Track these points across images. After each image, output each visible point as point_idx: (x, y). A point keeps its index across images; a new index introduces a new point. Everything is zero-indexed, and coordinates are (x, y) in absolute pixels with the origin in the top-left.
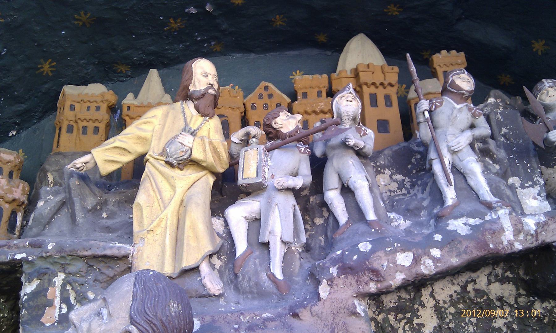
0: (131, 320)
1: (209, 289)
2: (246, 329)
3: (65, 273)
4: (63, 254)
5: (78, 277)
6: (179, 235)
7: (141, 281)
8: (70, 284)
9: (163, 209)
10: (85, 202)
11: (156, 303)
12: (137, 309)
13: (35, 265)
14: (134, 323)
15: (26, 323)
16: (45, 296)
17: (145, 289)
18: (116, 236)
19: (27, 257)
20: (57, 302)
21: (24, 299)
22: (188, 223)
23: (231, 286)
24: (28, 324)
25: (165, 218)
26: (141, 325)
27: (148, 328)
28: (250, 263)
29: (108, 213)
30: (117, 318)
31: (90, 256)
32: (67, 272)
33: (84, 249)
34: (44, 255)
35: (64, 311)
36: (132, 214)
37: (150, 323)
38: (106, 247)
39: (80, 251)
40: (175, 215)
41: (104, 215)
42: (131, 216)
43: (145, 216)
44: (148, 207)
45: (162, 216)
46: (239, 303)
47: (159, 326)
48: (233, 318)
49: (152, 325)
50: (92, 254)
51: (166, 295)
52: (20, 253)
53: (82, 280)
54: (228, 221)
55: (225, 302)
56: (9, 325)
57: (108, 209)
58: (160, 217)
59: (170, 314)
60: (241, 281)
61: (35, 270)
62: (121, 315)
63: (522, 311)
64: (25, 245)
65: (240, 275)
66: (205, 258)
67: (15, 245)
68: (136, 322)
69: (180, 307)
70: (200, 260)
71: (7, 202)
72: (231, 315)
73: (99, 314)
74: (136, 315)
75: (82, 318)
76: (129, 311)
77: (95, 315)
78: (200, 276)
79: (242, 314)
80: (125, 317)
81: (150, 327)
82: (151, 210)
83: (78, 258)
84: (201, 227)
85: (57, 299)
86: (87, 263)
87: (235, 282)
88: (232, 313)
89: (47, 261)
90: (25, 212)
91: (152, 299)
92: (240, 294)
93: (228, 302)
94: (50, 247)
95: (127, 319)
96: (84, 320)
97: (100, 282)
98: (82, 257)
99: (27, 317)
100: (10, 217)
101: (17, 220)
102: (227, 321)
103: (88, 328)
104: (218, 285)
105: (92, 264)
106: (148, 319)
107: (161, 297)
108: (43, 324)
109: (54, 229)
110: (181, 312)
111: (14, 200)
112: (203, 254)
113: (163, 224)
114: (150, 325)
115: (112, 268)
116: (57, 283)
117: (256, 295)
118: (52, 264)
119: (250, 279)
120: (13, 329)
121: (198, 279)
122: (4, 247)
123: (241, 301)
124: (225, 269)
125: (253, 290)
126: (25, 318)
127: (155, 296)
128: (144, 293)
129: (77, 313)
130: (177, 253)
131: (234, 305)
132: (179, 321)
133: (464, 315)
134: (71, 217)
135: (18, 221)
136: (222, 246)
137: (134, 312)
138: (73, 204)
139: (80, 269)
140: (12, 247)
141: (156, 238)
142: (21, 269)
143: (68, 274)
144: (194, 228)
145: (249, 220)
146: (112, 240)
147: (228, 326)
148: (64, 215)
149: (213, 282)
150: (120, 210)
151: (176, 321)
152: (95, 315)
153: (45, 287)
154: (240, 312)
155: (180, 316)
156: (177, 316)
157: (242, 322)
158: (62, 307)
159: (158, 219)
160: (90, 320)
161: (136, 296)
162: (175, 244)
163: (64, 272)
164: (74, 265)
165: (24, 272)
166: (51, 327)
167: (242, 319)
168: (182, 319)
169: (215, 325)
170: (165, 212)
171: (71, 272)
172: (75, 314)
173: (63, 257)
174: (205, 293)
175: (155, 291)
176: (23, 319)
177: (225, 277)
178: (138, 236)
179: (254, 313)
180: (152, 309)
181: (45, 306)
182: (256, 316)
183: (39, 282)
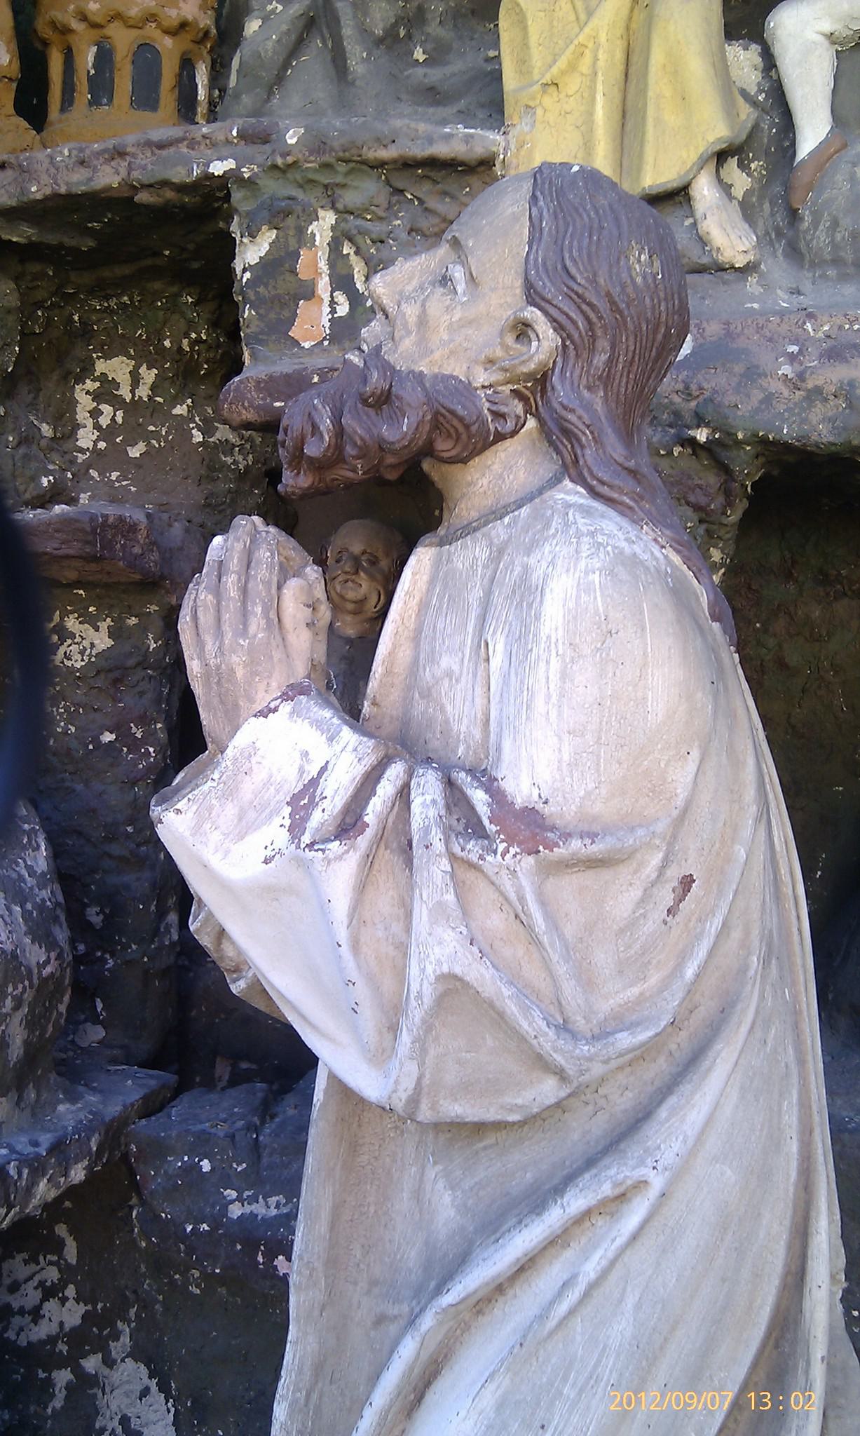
0: (529, 292)
1: (719, 249)
2: (821, 356)
3: (337, 211)
4: (327, 158)
5: (370, 220)
6: (629, 97)
7: (550, 188)
8: (350, 240)
9: (583, 17)
10: (365, 14)
11: (593, 249)
12: (544, 263)
13: (259, 189)
14: (538, 300)
15: (257, 339)
16: (294, 272)
17: (562, 210)
18: (455, 110)
19: (238, 168)
20: (323, 286)
21: (244, 280)
22: (657, 57)
23: (777, 246)
24: (260, 342)
25: (591, 45)
26: (556, 307)
27: (573, 315)
28: (839, 177)
29: (429, 46)
30: (492, 290)
31: (395, 161)
32: (340, 206)
33: (378, 140)
34: (279, 161)
35: (343, 309)
36: (496, 44)
37: (579, 299)
38: (435, 136)
39: (369, 148)
40: (619, 35)
41: (419, 55)
42: (492, 53)
43: (533, 39)
44: (542, 14)
45: (581, 38)
46: (799, 293)
47: (601, 310)
48: (785, 327)
49: (584, 307)
50: (401, 157)
51: (619, 227)
52: (220, 159)
53: (378, 229)
54: (777, 50)
55: (762, 286)
56: (214, 363)
57: (429, 34)
58: (576, 42)
59: (633, 281)
60: (809, 229)
61: (263, 203)
62: (500, 281)
63: (766, 1396)
64: (230, 138)
65: (807, 213)
66: (707, 160)
67: (204, 137)
68: (543, 299)
69: (657, 264)
70: (691, 168)
71: (167, 32)
72: (779, 320)
73: (445, 280)
74: (541, 279)
75: (401, 293)
76: (521, 270)
77: (433, 284)
78: (692, 213)
79: (811, 316)
80: (512, 287)
81: (579, 313)
82: (551, 22)
83: (364, 167)
84: (697, 67)
85: (322, 279)
86: (388, 182)
87: (791, 233)
88: (782, 314)
89: (288, 179)
90: (214, 62)
91: (582, 235)
92: (802, 267)
93: (767, 286)
94: (291, 140)
95: (518, 291)
96: (408, 298)
97: (426, 236)
98: (374, 164)
99: (257, 326)
100: (180, 75)
101: (197, 85)
102: (768, 334)
103: (419, 317)
104: (743, 239)
105: (400, 185)
106: (573, 290)
107: (605, 232)
108: (297, 343)
109: (292, 99)
110: (660, 277)
111: (184, 25)
112: (701, 150)
113: (585, 65)
114: (579, 307)
115: (453, 197)
116: (318, 238)
117: (851, 270)
118: (301, 186)
119: (835, 224)
120: (223, 372)
121: (688, 222)
122: (180, 145)
123: (807, 286)
124: (761, 198)
125: (842, 254)
126: (253, 329)
127: (591, 228)
128: (561, 222)
129: (388, 278)
130: (625, 151)
131: (786, 297)
132: (655, 301)
133: (616, 1406)
134: (334, 60)
135: (200, 87)
136: (756, 128)
137: (537, 272)
138: (337, 20)
139: (373, 197)
140: (199, 143)
141: (568, 108)
142: (226, 205)
143: (343, 213)
144: (675, 70)
145: (840, 44)
146: (444, 122)
147: (770, 348)
148: (313, 59)
149: (729, 230)
150: (460, 38)
151: (648, 300)
152: (433, 284)
153: (291, 249)
154: (804, 312)
155: (656, 287)
156: (648, 287)
157: (809, 338)
158: (336, 300)
159: (572, 47)
160: (422, 297)
161: (538, 229)
162: (621, 123)
163: (333, 207)
164: (356, 188)
165: (236, 210)
166: (316, 350)
167: (810, 330)
168: (662, 295)
169: (735, 346)
170: (591, 25)
171: (350, 206)
172: (384, 283)
173: (326, 166)
174: (705, 260)
175: (589, 216)
176: (248, 331)
177: (761, 223)
178: (516, 103)
179: (845, 315)
180: (583, 264)
181: (296, 299)
182: (851, 323)
183: (274, 237)
